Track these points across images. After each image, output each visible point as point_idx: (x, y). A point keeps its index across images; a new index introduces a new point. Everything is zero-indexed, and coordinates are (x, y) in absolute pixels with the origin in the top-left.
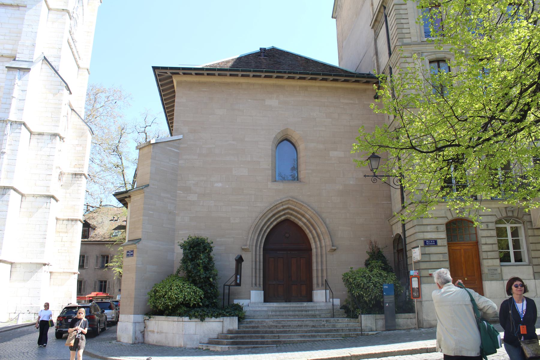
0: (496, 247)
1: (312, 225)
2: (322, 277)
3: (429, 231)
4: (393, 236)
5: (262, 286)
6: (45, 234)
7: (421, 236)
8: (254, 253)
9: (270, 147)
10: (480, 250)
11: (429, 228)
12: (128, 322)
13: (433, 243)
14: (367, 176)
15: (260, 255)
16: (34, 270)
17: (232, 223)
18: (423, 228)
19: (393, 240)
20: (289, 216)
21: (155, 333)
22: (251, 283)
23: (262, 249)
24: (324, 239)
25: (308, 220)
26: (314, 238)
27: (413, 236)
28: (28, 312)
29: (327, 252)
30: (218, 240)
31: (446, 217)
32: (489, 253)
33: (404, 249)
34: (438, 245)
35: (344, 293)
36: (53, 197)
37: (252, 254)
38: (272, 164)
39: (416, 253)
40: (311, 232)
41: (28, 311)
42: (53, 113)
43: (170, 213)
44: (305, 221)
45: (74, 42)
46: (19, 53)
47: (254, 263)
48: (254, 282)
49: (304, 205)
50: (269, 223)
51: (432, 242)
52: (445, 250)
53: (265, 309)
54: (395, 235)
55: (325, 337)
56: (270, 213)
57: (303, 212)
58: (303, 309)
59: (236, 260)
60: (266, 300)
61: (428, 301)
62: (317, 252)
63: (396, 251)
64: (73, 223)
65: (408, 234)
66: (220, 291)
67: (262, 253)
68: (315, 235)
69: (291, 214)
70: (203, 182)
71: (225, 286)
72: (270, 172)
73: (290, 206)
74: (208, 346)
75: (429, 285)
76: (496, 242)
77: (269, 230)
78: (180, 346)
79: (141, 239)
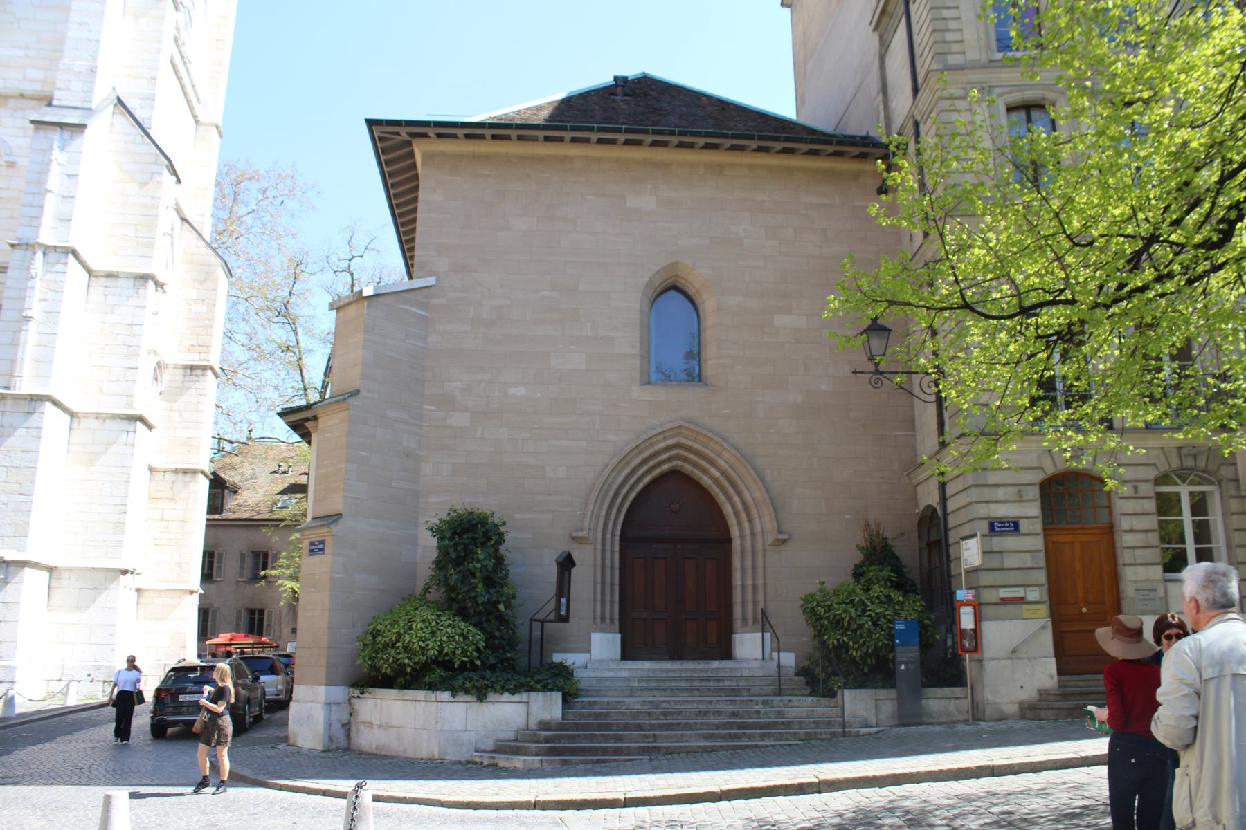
0: (1154, 538)
2: (755, 602)
3: (1002, 498)
4: (917, 511)
5: (617, 622)
7: (983, 510)
8: (599, 547)
10: (1118, 545)
11: (1000, 493)
12: (312, 702)
15: (612, 552)
16: (101, 585)
18: (987, 494)
20: (679, 463)
22: (592, 616)
23: (617, 538)
25: (723, 473)
26: (736, 514)
27: (963, 510)
28: (90, 679)
29: (766, 546)
30: (517, 516)
31: (1041, 468)
32: (1138, 552)
35: (804, 639)
36: (142, 419)
37: (595, 549)
39: (969, 549)
40: (729, 499)
41: (89, 675)
46: (59, 89)
49: (715, 438)
50: (633, 479)
51: (1007, 524)
52: (1038, 543)
53: (624, 674)
54: (922, 508)
56: (636, 456)
57: (712, 455)
59: (558, 563)
60: (627, 654)
62: (743, 546)
63: (923, 545)
64: (188, 477)
65: (952, 505)
67: (617, 548)
68: (740, 507)
69: (685, 460)
71: (534, 623)
73: (683, 440)
74: (494, 758)
76: (1156, 526)
77: (633, 495)
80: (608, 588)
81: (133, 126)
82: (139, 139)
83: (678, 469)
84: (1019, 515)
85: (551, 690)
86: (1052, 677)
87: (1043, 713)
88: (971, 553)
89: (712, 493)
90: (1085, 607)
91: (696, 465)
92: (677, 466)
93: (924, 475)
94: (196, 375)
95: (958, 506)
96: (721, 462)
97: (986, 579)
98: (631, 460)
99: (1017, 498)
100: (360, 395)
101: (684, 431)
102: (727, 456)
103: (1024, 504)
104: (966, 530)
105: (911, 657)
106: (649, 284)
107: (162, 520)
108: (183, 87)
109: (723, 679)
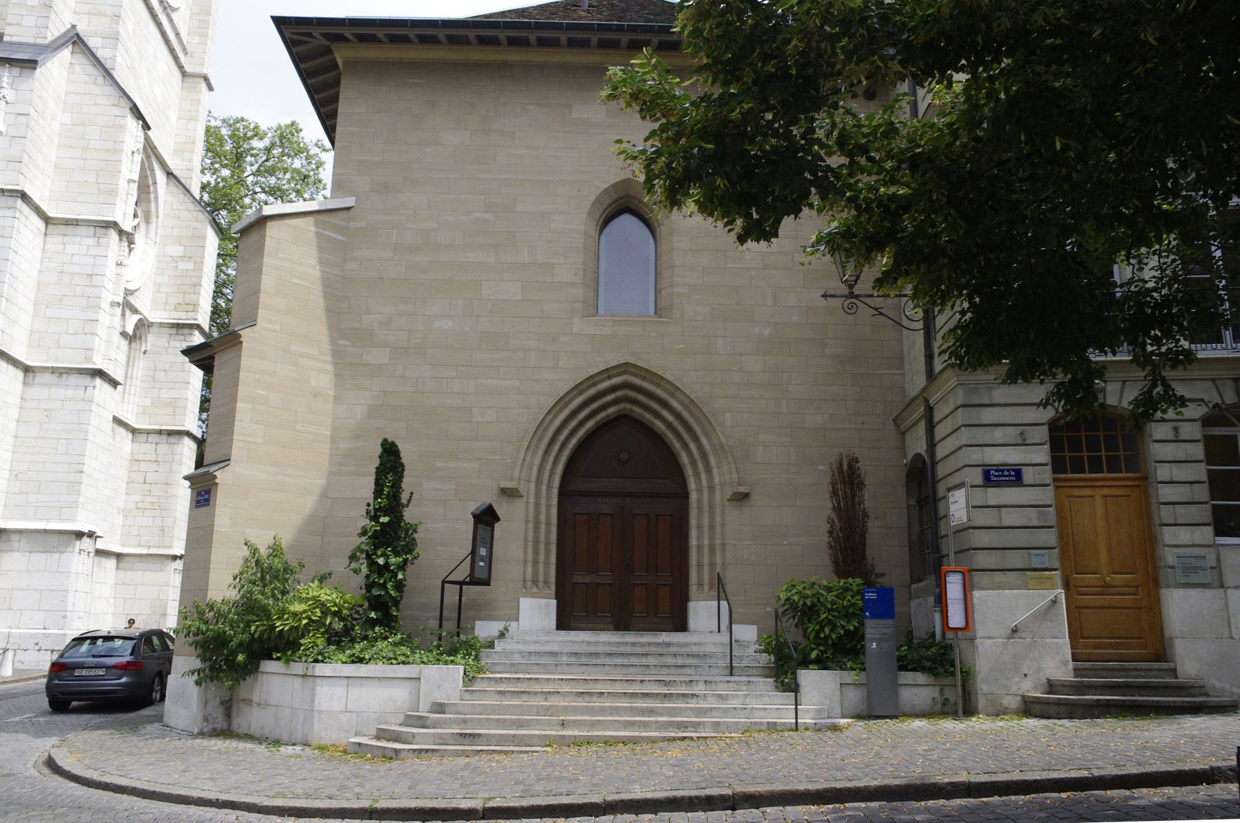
0: (1202, 492)
2: (712, 565)
3: (1000, 442)
4: (905, 461)
5: (553, 587)
6: (81, 462)
7: (975, 456)
8: (532, 500)
10: (1153, 500)
11: (998, 435)
13: (1010, 476)
14: (830, 296)
15: (548, 507)
16: (54, 547)
18: (981, 435)
20: (628, 406)
21: (255, 705)
22: (522, 579)
23: (555, 491)
27: (953, 456)
28: (37, 647)
32: (1180, 509)
34: (1024, 483)
35: (768, 609)
36: (99, 373)
38: (584, 270)
39: (957, 501)
41: (37, 644)
42: (100, 173)
45: (165, 8)
46: (10, 24)
47: (531, 525)
51: (1006, 473)
54: (910, 457)
59: (475, 516)
60: (563, 623)
62: (700, 501)
63: (913, 502)
64: (172, 439)
65: (941, 452)
67: (555, 502)
68: (697, 456)
69: (635, 402)
70: (406, 317)
71: (446, 585)
72: (579, 292)
76: (1204, 477)
80: (542, 547)
81: (95, 65)
82: (101, 80)
83: (622, 413)
84: (1023, 462)
88: (957, 507)
89: (667, 441)
92: (625, 409)
93: (912, 418)
95: (947, 452)
99: (1020, 441)
104: (956, 479)
105: (884, 634)
106: (597, 201)
108: (163, 34)
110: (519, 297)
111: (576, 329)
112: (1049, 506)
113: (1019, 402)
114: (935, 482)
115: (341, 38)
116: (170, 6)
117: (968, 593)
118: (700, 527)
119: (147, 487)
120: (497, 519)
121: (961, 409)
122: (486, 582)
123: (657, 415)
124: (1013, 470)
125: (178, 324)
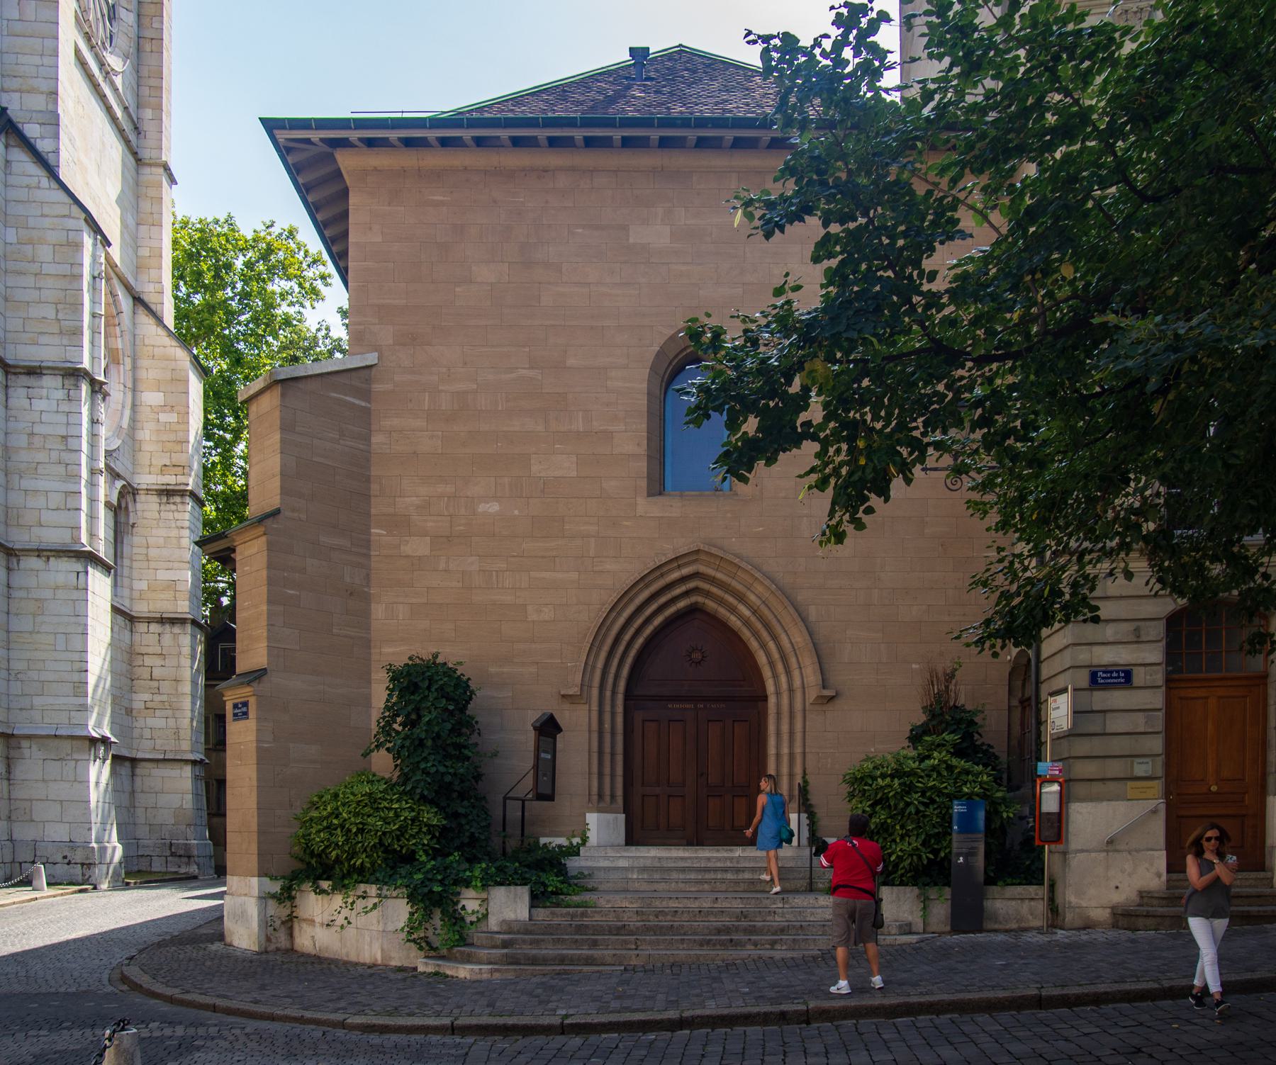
1: (767, 626)
2: (791, 775)
3: (1111, 639)
4: (1009, 658)
5: (620, 800)
7: (1084, 656)
8: (595, 707)
9: (645, 385)
12: (246, 895)
13: (1119, 677)
16: (67, 755)
17: (533, 622)
19: (1008, 669)
20: (700, 599)
21: (317, 925)
24: (800, 668)
25: (755, 612)
26: (772, 664)
27: (1058, 655)
28: (66, 861)
29: (807, 704)
30: (492, 670)
33: (1033, 698)
37: (590, 710)
39: (1058, 708)
40: (763, 646)
41: (65, 857)
42: (60, 306)
43: (351, 594)
44: (747, 613)
48: (595, 789)
49: (743, 565)
50: (639, 621)
51: (1115, 675)
52: (1156, 699)
53: (623, 863)
55: (768, 946)
56: (641, 590)
57: (739, 587)
58: (729, 864)
59: (535, 728)
60: (632, 839)
61: (1087, 851)
62: (778, 705)
63: (1015, 702)
66: (497, 813)
67: (620, 709)
68: (776, 656)
69: (708, 594)
72: (643, 465)
73: (702, 569)
74: (439, 965)
75: (1094, 804)
77: (640, 641)
78: (373, 961)
79: (265, 669)
84: (1133, 662)
85: (509, 885)
86: (1159, 876)
87: (1141, 922)
89: (743, 638)
90: (1216, 784)
91: (721, 602)
92: (696, 603)
94: (174, 503)
95: (1054, 650)
96: (752, 597)
97: (1082, 747)
98: (636, 595)
100: (281, 516)
101: (703, 557)
102: (759, 589)
103: (1142, 646)
104: (1059, 683)
107: (151, 679)
109: (743, 870)
110: (574, 474)
111: (640, 510)
112: (1159, 710)
113: (1135, 594)
114: (1038, 683)
115: (343, 143)
116: (113, 70)
117: (1064, 805)
118: (778, 734)
119: (155, 684)
120: (560, 730)
121: (1070, 650)
122: (550, 798)
123: (733, 610)
124: (1123, 671)
125: (166, 490)
